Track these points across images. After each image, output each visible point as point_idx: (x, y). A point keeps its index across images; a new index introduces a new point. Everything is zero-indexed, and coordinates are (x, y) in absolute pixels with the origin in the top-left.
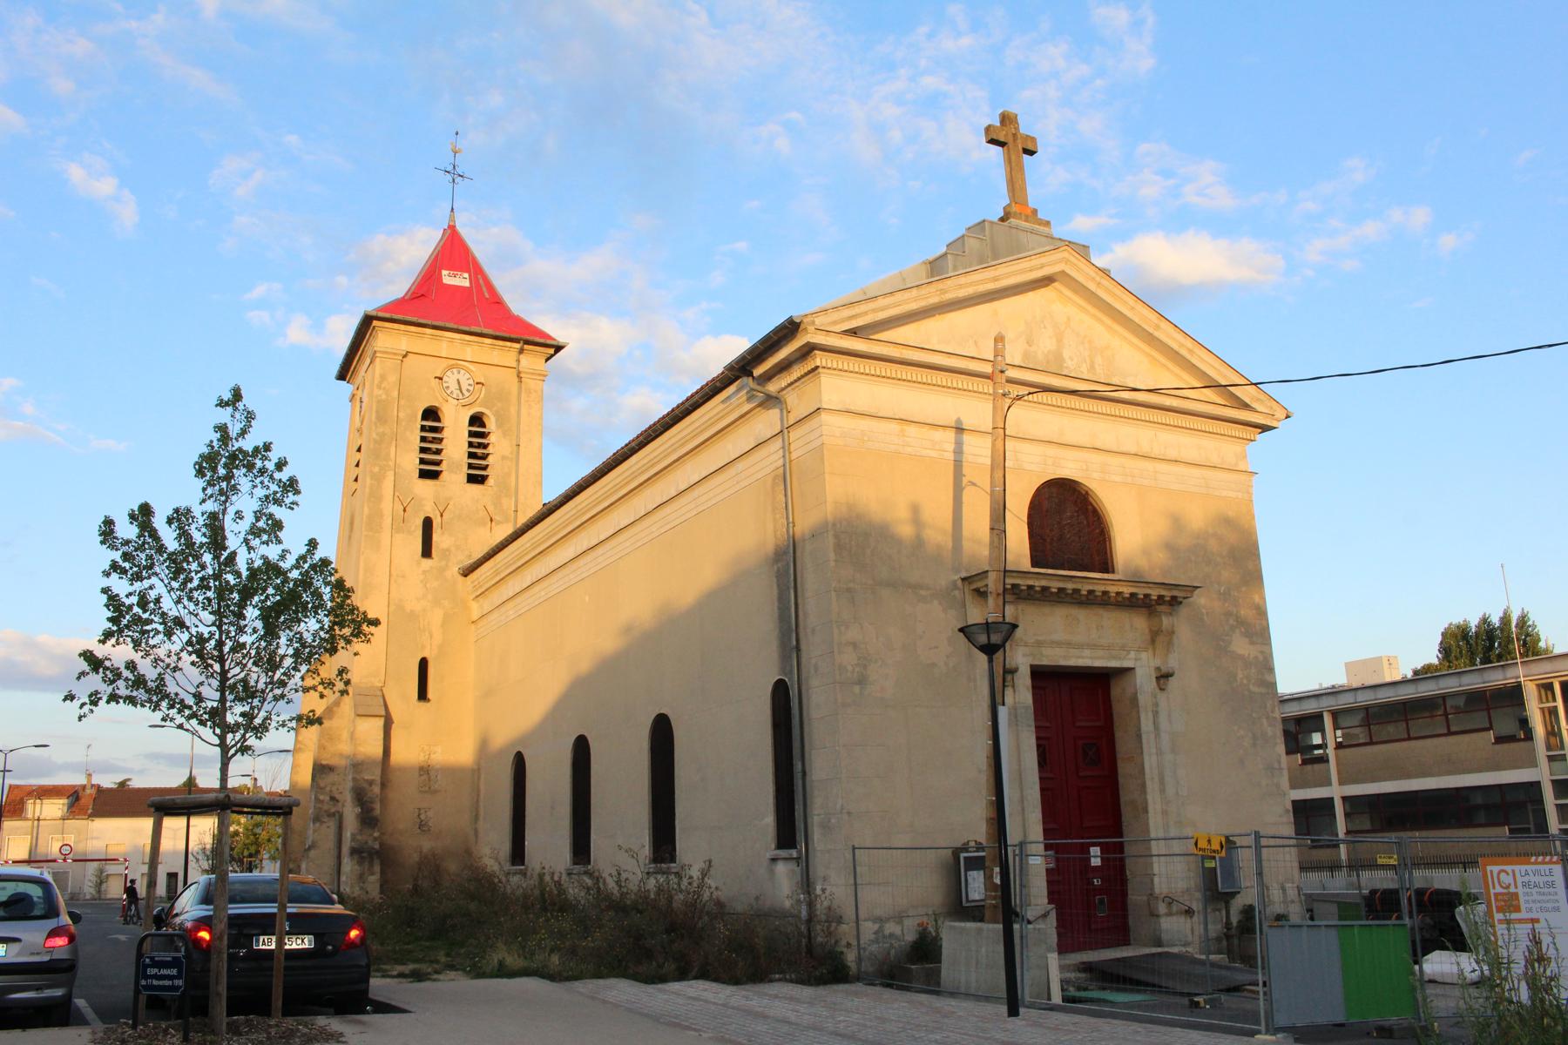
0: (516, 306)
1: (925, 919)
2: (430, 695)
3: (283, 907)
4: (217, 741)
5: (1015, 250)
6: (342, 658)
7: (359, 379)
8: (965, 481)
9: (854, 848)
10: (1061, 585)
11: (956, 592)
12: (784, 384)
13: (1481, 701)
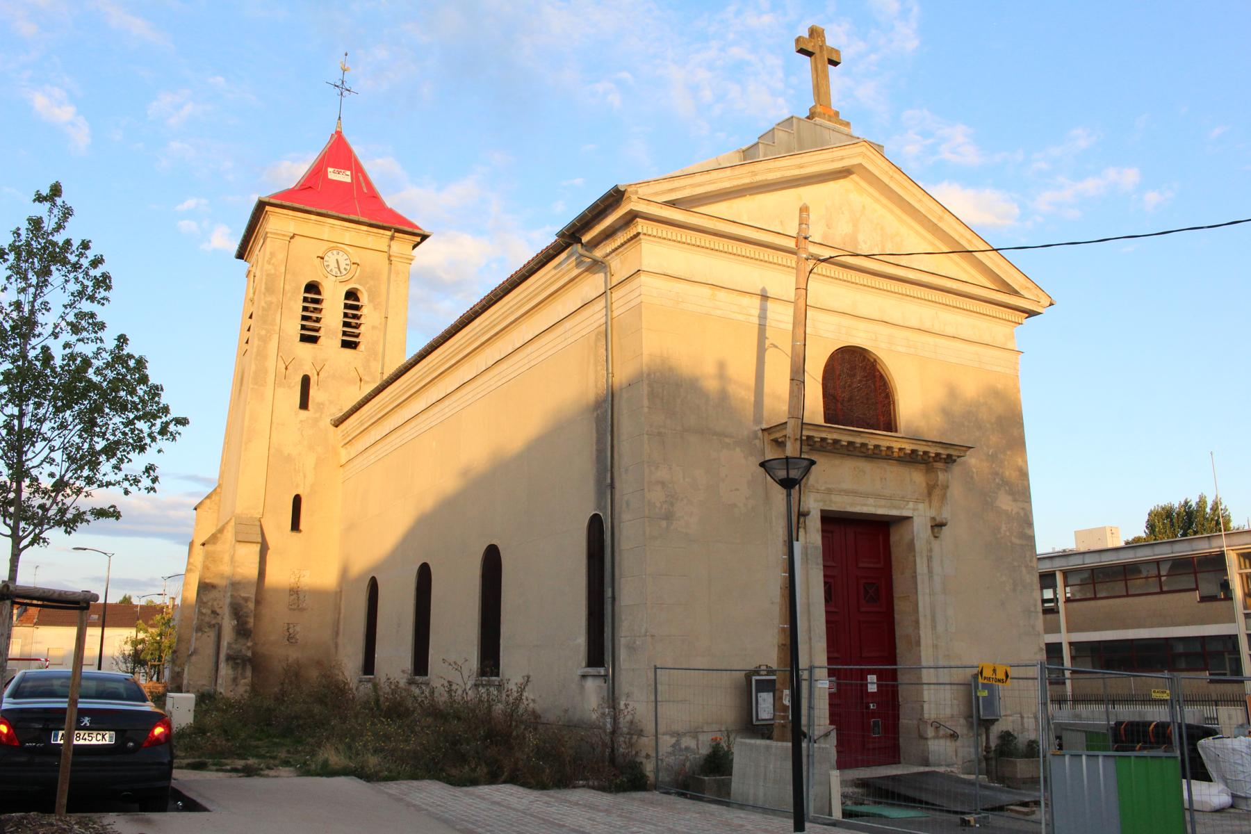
0: (390, 201)
1: (718, 735)
2: (302, 527)
3: (74, 702)
4: (9, 532)
5: (820, 145)
6: (150, 456)
7: (254, 259)
8: (767, 343)
9: (656, 668)
10: (851, 439)
11: (757, 442)
12: (609, 250)
13: (1182, 566)
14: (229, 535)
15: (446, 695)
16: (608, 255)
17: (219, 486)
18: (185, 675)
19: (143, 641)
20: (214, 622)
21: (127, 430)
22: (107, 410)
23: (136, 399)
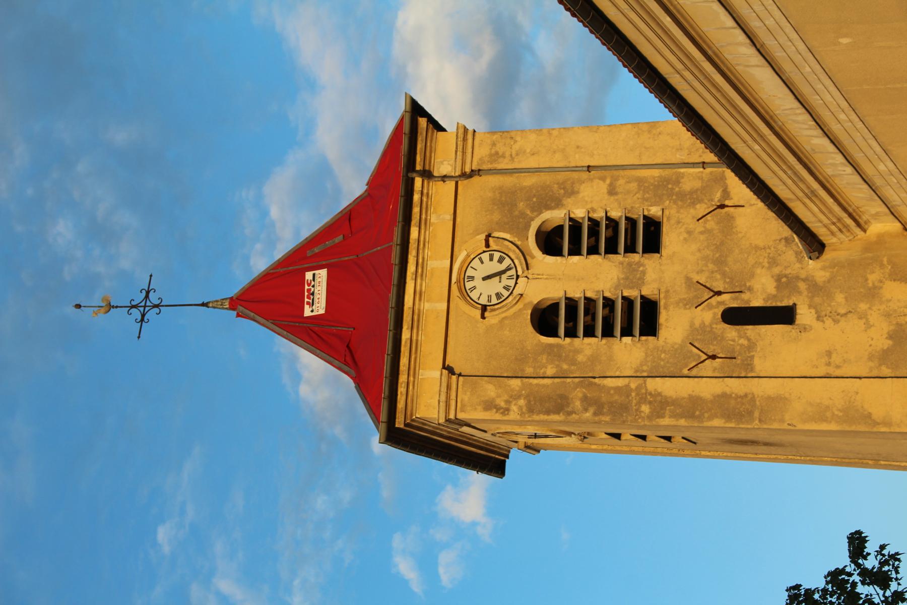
0: (354, 186)
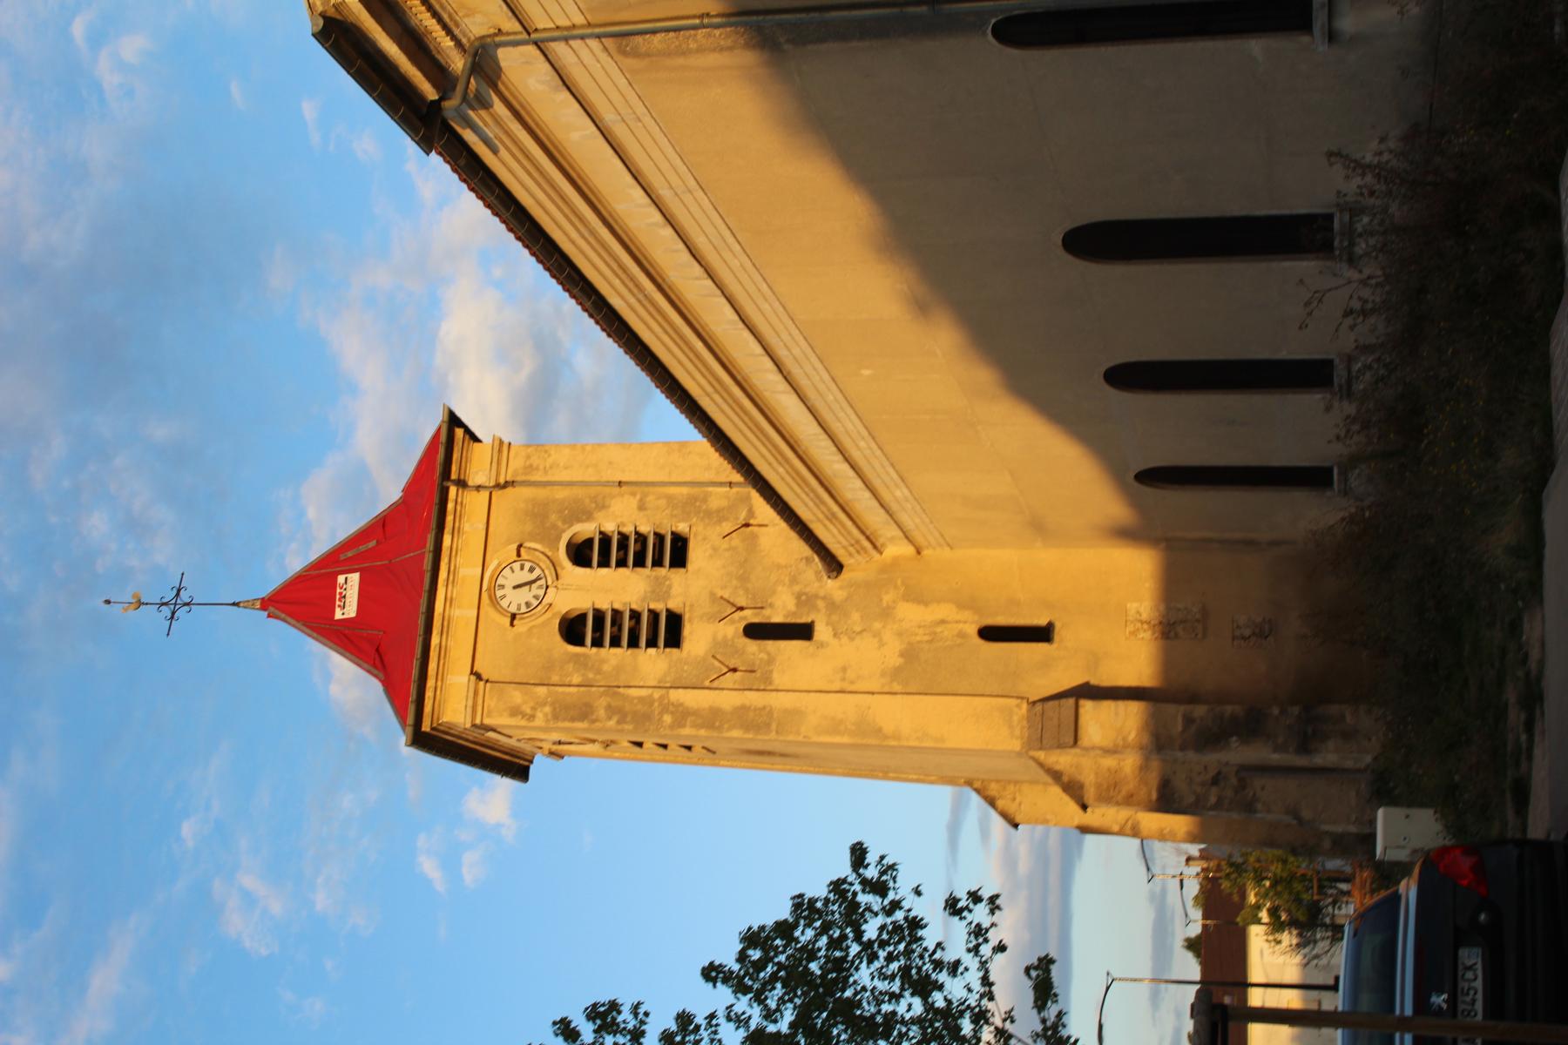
0: (390, 492)
3: (1404, 1024)
6: (929, 909)
7: (527, 747)
12: (448, 43)
14: (1063, 760)
15: (1372, 320)
16: (459, 44)
17: (969, 783)
18: (1338, 829)
19: (1273, 912)
20: (1234, 781)
21: (882, 954)
22: (848, 993)
23: (824, 940)
